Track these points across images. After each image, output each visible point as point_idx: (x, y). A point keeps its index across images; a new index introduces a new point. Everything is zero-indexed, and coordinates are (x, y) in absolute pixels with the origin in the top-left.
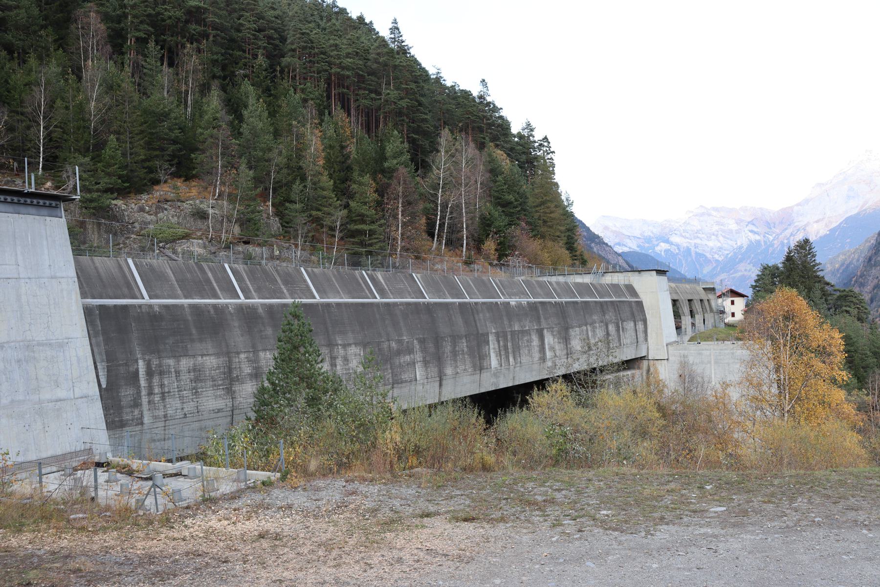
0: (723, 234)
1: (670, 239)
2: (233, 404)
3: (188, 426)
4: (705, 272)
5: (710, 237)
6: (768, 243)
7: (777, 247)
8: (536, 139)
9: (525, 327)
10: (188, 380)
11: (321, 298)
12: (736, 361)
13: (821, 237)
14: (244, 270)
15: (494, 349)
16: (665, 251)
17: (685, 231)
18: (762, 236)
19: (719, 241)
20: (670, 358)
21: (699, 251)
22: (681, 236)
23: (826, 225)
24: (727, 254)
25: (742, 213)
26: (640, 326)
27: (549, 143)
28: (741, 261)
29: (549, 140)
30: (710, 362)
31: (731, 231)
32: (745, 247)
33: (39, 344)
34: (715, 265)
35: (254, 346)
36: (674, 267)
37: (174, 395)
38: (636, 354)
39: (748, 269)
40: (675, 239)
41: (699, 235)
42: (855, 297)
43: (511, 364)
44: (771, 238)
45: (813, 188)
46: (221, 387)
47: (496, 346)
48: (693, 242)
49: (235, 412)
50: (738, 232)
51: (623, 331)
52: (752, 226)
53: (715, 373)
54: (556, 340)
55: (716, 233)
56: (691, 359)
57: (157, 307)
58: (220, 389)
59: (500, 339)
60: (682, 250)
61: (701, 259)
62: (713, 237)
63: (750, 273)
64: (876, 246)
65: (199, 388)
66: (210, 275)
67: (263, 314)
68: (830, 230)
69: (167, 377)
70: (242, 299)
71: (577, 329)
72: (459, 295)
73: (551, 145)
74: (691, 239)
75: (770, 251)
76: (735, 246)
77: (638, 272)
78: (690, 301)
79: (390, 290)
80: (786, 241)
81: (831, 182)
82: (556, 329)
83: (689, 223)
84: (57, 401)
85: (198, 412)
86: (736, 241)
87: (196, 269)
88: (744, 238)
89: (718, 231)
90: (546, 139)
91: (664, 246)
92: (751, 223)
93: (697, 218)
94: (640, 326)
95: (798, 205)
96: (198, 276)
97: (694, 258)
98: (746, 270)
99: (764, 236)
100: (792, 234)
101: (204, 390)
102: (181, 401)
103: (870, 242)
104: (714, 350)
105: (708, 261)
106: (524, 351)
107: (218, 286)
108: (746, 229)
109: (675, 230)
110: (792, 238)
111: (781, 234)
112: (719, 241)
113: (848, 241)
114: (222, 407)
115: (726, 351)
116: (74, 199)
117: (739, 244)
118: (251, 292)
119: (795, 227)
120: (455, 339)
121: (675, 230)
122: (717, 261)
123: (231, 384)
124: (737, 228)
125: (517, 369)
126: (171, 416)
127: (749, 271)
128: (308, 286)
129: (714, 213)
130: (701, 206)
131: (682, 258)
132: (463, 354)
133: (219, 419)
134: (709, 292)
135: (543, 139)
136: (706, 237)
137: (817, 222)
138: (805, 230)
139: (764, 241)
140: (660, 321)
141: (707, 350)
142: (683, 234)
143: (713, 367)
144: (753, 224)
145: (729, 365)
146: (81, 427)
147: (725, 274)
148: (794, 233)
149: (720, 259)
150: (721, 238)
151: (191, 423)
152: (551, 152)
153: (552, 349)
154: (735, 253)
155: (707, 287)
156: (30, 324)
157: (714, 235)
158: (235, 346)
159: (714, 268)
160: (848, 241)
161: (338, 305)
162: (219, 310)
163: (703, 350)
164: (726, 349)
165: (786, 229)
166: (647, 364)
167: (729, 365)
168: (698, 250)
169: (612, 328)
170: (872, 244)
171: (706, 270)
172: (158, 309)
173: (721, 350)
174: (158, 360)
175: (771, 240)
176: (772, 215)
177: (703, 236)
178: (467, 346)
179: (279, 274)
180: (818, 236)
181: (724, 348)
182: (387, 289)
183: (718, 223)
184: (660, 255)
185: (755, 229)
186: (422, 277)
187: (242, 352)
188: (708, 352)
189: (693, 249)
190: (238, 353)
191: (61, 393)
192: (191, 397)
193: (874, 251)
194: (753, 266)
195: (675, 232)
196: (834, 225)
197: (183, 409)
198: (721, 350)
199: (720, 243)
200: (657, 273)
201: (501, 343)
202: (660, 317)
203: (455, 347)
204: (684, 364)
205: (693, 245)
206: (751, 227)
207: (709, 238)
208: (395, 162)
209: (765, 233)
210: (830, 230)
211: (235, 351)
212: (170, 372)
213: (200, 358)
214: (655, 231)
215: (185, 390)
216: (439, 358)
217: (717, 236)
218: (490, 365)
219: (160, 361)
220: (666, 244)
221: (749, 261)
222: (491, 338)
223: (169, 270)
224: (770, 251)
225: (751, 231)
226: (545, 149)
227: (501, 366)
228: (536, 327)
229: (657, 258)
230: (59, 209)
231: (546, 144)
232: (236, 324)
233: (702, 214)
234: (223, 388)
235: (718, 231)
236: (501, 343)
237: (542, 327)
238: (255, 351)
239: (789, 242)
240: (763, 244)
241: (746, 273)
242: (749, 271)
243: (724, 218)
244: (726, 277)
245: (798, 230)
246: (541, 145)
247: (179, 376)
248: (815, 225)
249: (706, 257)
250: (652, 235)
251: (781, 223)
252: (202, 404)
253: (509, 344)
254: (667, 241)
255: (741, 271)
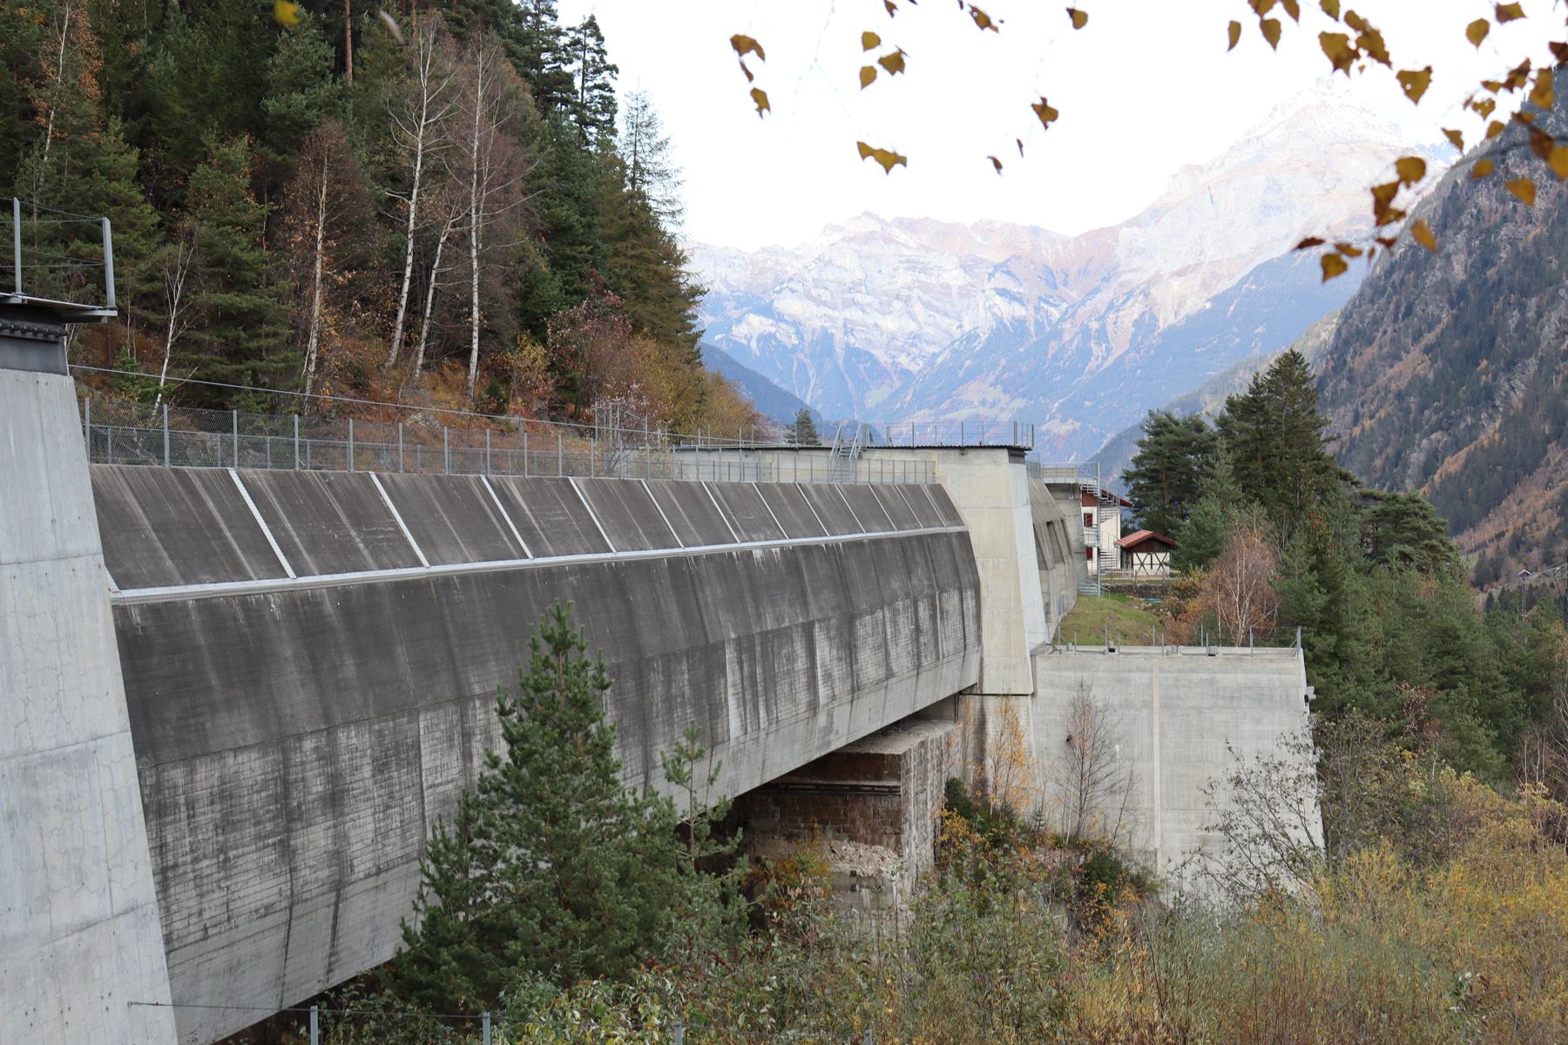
0: (926, 297)
1: (776, 304)
2: (292, 889)
3: (208, 965)
4: (870, 403)
5: (890, 305)
6: (1048, 329)
7: (1071, 341)
8: (562, 23)
9: (783, 621)
10: (211, 827)
11: (432, 563)
12: (1220, 702)
13: (1188, 317)
14: (270, 486)
15: (734, 685)
16: (758, 340)
17: (817, 283)
18: (1030, 306)
19: (913, 317)
20: (1040, 692)
21: (857, 341)
22: (808, 296)
23: (1205, 286)
24: (935, 355)
25: (979, 240)
26: (970, 603)
27: (601, 39)
28: (972, 375)
29: (603, 32)
30: (1148, 704)
31: (947, 288)
32: (984, 337)
33: (48, 761)
34: (898, 384)
35: (327, 716)
36: (783, 386)
37: (185, 873)
38: (961, 680)
39: (990, 399)
40: (789, 305)
41: (858, 297)
42: (1425, 517)
43: (762, 726)
44: (1056, 314)
45: (1175, 176)
46: (270, 841)
47: (738, 676)
48: (840, 315)
49: (298, 910)
50: (965, 292)
51: (942, 618)
52: (1006, 277)
53: (1162, 735)
54: (834, 652)
55: (905, 292)
56: (1098, 696)
57: (137, 611)
58: (268, 846)
59: (744, 657)
60: (808, 337)
61: (861, 367)
62: (897, 305)
63: (996, 410)
64: (1336, 348)
65: (232, 848)
66: (211, 505)
67: (334, 618)
68: (1214, 297)
69: (171, 823)
70: (291, 580)
71: (868, 618)
72: (662, 540)
73: (605, 46)
74: (835, 308)
75: (1051, 352)
76: (957, 333)
77: (957, 452)
78: (1049, 524)
79: (542, 529)
80: (1094, 325)
81: (1223, 164)
82: (833, 621)
83: (830, 261)
84: (82, 930)
85: (229, 919)
86: (959, 318)
87: (176, 481)
88: (981, 310)
89: (909, 288)
90: (591, 26)
91: (756, 324)
92: (1004, 268)
93: (853, 245)
94: (970, 603)
95: (1131, 223)
96: (189, 510)
97: (840, 362)
98: (983, 402)
99: (1038, 309)
100: (1111, 306)
101: (240, 851)
102: (198, 891)
103: (1318, 336)
104: (1162, 670)
105: (878, 372)
106: (783, 688)
107: (235, 537)
108: (988, 287)
109: (791, 280)
110: (1112, 316)
111: (1083, 303)
112: (913, 317)
113: (1260, 329)
114: (272, 899)
115: (1194, 676)
116: (100, 318)
117: (967, 327)
118: (299, 552)
119: (1121, 285)
120: (669, 659)
121: (791, 280)
122: (905, 373)
123: (288, 830)
124: (961, 282)
125: (772, 737)
126: (179, 938)
127: (993, 404)
128: (399, 531)
129: (902, 236)
130: (867, 214)
131: (807, 361)
132: (683, 704)
133: (267, 933)
134: (1062, 495)
135: (585, 27)
136: (876, 304)
137: (1180, 273)
138: (1146, 295)
139: (1037, 322)
140: (1018, 588)
141: (1144, 671)
142: (814, 292)
143: (1156, 717)
144: (1008, 273)
145: (1200, 713)
146: (127, 1000)
147: (926, 411)
148: (1116, 304)
149: (914, 368)
150: (918, 309)
151: (214, 955)
152: (607, 68)
153: (828, 676)
154: (954, 351)
155: (1060, 480)
156: (27, 701)
157: (898, 297)
158: (292, 716)
159: (897, 392)
160: (1260, 329)
161: (465, 578)
162: (251, 606)
163: (1130, 671)
164: (1193, 671)
165: (1096, 291)
166: (978, 705)
167: (1200, 713)
168: (852, 340)
169: (924, 612)
170: (1325, 342)
171: (876, 397)
172: (139, 620)
173: (1179, 671)
174: (153, 771)
175: (1054, 320)
176: (1060, 247)
177: (869, 299)
178: (689, 680)
179: (336, 495)
180: (1183, 313)
181: (1188, 665)
182: (537, 526)
183: (912, 265)
184: (746, 349)
185: (1013, 288)
186: (586, 483)
187: (306, 733)
188: (1145, 677)
189: (839, 335)
190: (299, 738)
191: (91, 906)
192: (216, 876)
193: (1332, 363)
194: (1004, 392)
195: (791, 285)
196: (1225, 285)
197: (200, 913)
198: (1179, 671)
199: (915, 320)
200: (1011, 455)
201: (746, 669)
202: (1017, 577)
203: (669, 687)
204: (1082, 709)
205: (840, 323)
206: (1001, 281)
207: (885, 309)
208: (299, 99)
209: (1040, 298)
210: (1214, 299)
211: (294, 732)
212: (176, 805)
213: (230, 760)
214: (733, 278)
215: (205, 857)
216: (644, 720)
217: (907, 301)
218: (728, 730)
219: (158, 775)
220: (762, 318)
221: (992, 378)
222: (730, 655)
223: (131, 495)
224: (1051, 352)
225: (1003, 293)
226: (588, 57)
227: (746, 733)
228: (801, 620)
229: (736, 357)
230: (59, 348)
231: (591, 42)
232: (288, 651)
233: (869, 238)
234: (274, 844)
235: (909, 288)
236: (746, 669)
237: (811, 619)
238: (330, 731)
239: (1103, 326)
240: (1032, 329)
241: (982, 411)
242: (993, 404)
243: (928, 249)
244: (929, 420)
245: (1130, 295)
246: (575, 43)
247: (194, 816)
248: (1175, 284)
249: (875, 361)
250: (724, 291)
251: (1084, 272)
252: (236, 895)
253: (759, 670)
254: (767, 311)
255: (971, 405)
